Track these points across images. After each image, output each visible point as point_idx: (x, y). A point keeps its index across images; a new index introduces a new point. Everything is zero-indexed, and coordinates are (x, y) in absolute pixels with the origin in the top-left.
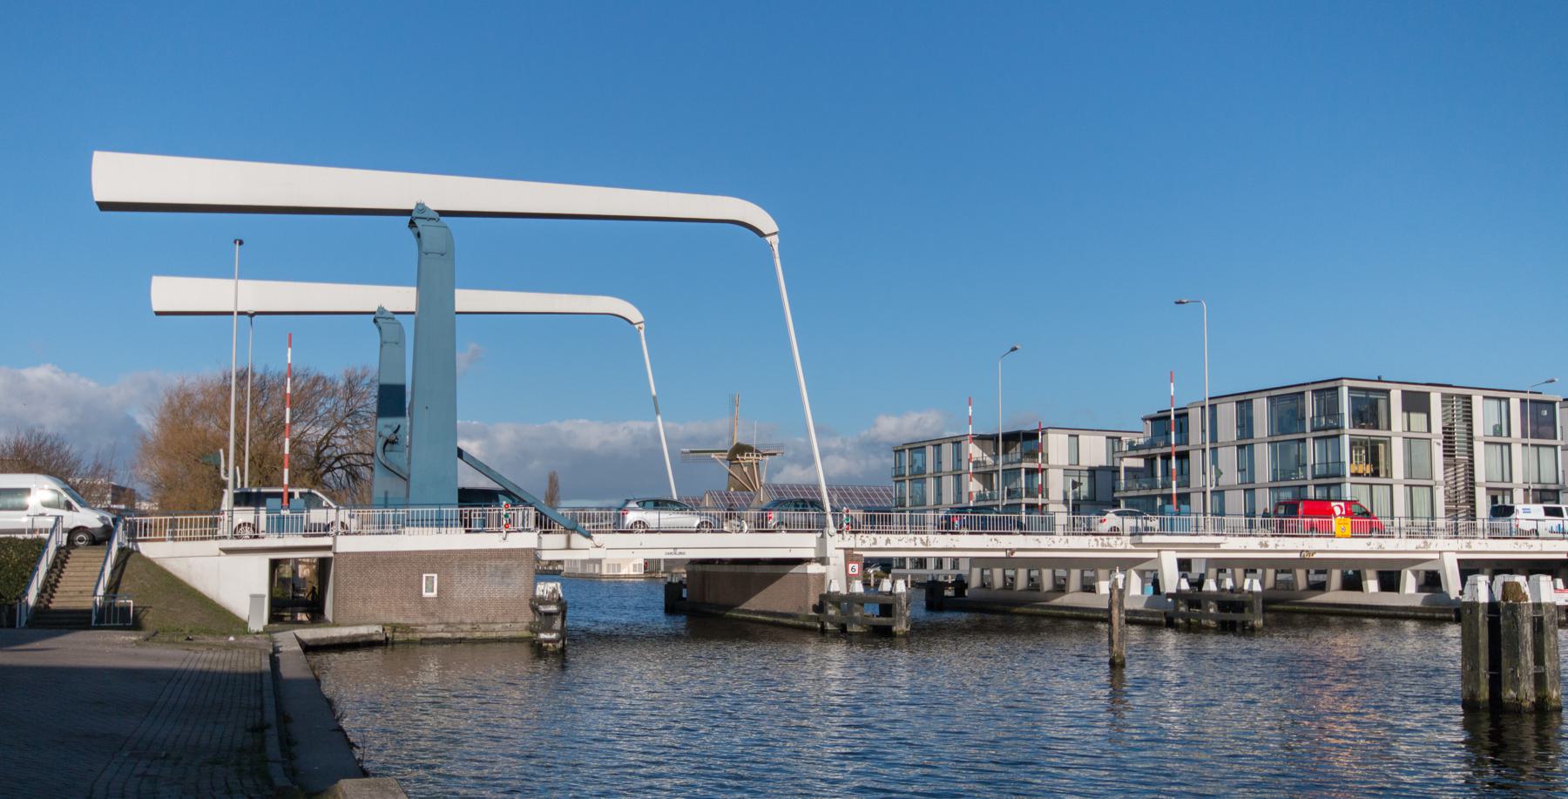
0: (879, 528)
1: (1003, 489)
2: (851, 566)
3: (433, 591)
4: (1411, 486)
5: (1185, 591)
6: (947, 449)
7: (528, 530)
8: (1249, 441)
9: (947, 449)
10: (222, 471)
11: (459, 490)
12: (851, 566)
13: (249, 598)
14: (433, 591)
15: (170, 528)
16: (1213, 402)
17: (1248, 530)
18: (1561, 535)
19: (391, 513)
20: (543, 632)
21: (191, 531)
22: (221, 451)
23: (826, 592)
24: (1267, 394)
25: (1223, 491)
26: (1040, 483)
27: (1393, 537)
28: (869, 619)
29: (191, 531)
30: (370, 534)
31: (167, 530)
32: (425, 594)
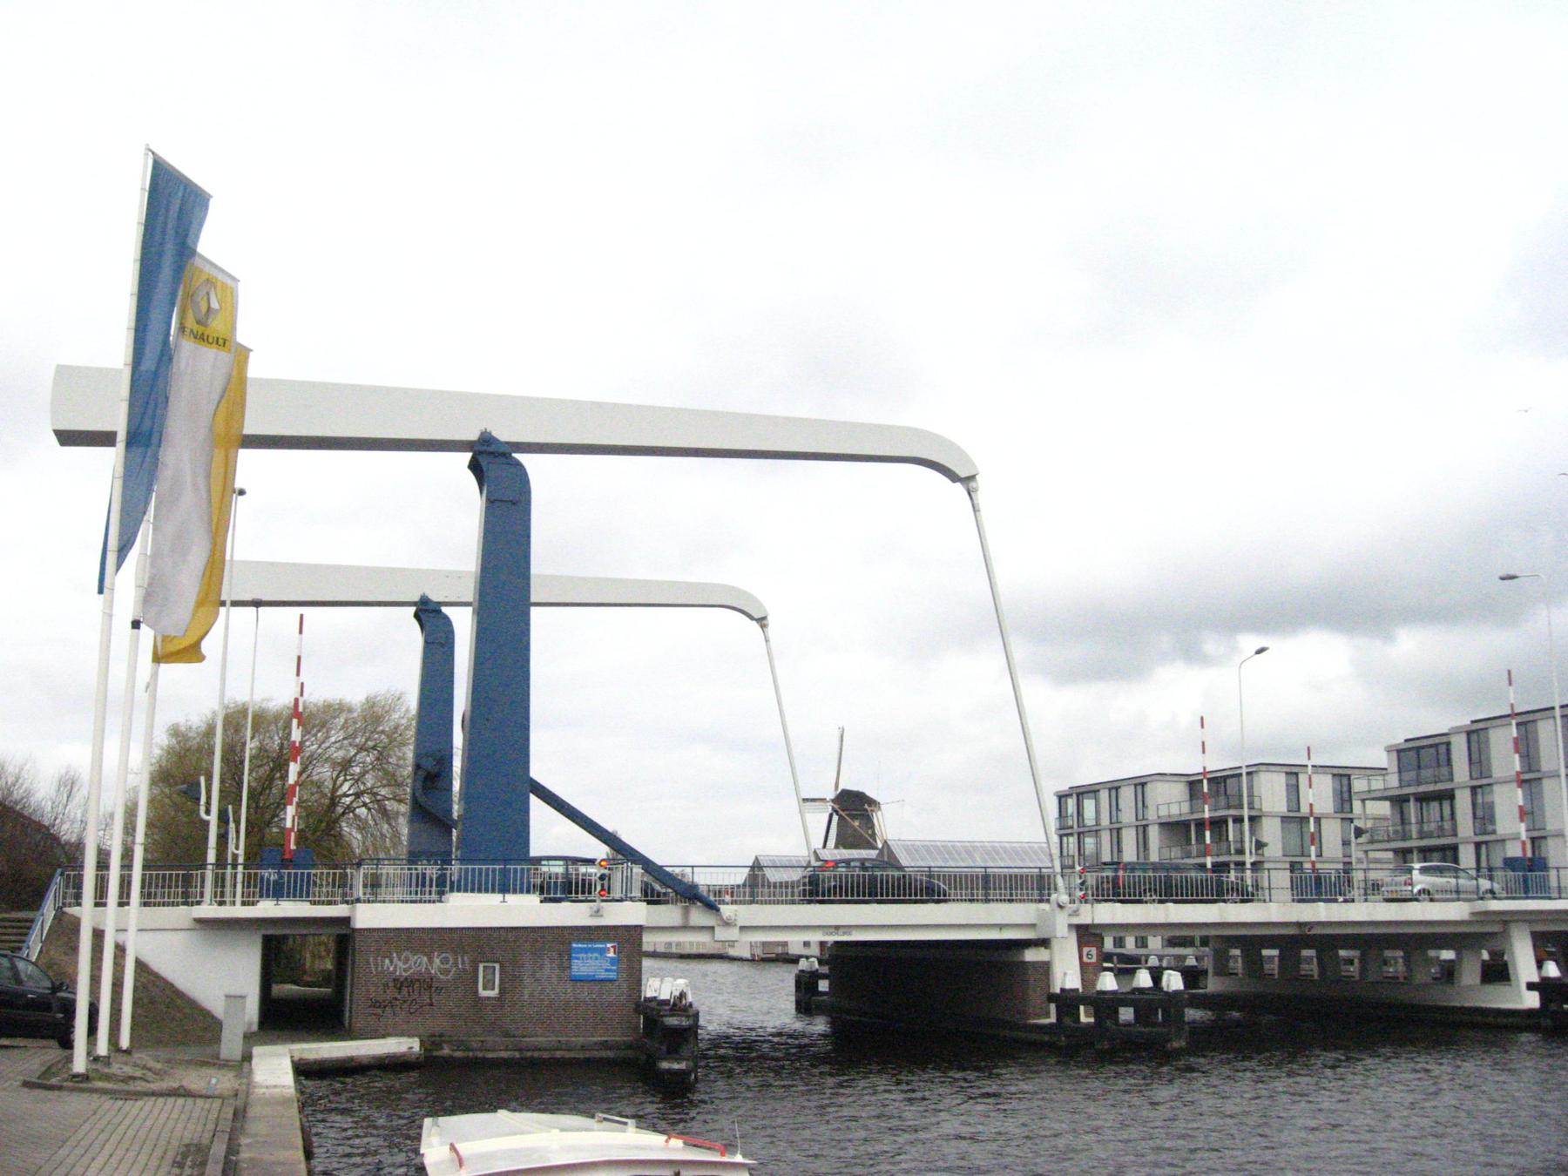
0: (1028, 894)
1: (1251, 842)
2: (1085, 950)
3: (493, 989)
4: (1303, 855)
5: (1554, 979)
6: (1127, 795)
7: (632, 899)
8: (1484, 781)
9: (1127, 795)
10: (202, 809)
11: (58, 366)
12: (1085, 950)
13: (223, 998)
14: (493, 989)
15: (437, 886)
16: (1250, 770)
17: (1036, 892)
18: (1454, 896)
19: (413, 872)
20: (665, 1059)
21: (169, 893)
22: (202, 779)
23: (1058, 991)
24: (1286, 769)
25: (1504, 840)
26: (1312, 830)
27: (1353, 901)
28: (1132, 1028)
29: (169, 893)
30: (402, 902)
31: (434, 889)
32: (483, 993)
